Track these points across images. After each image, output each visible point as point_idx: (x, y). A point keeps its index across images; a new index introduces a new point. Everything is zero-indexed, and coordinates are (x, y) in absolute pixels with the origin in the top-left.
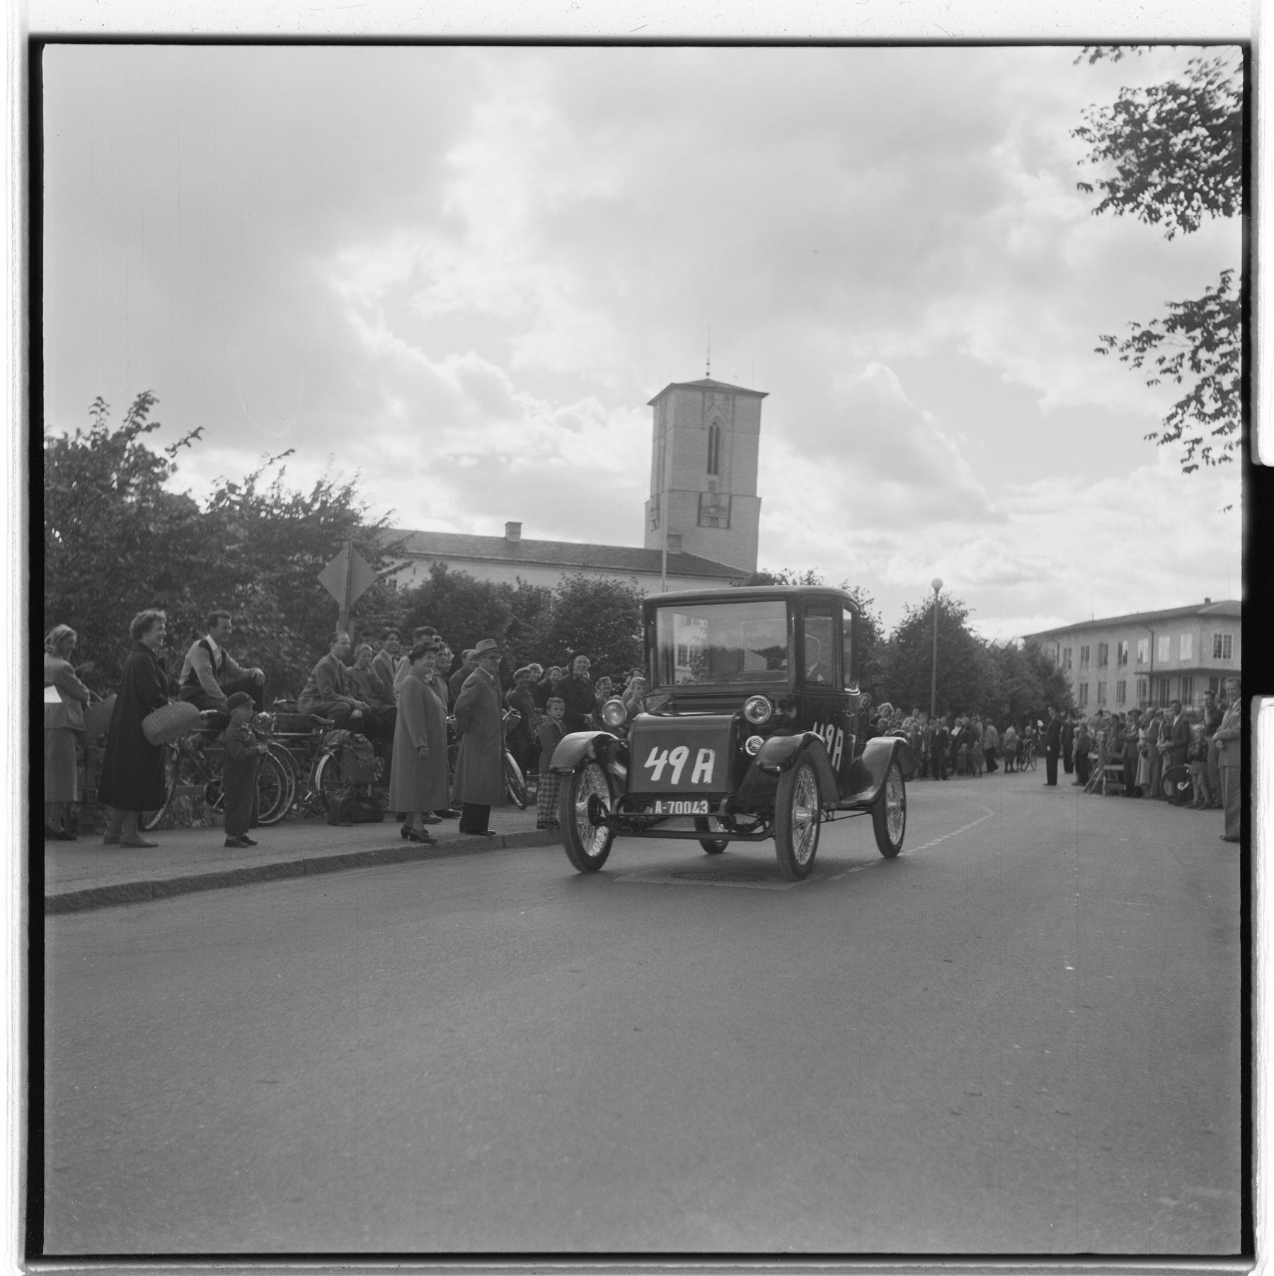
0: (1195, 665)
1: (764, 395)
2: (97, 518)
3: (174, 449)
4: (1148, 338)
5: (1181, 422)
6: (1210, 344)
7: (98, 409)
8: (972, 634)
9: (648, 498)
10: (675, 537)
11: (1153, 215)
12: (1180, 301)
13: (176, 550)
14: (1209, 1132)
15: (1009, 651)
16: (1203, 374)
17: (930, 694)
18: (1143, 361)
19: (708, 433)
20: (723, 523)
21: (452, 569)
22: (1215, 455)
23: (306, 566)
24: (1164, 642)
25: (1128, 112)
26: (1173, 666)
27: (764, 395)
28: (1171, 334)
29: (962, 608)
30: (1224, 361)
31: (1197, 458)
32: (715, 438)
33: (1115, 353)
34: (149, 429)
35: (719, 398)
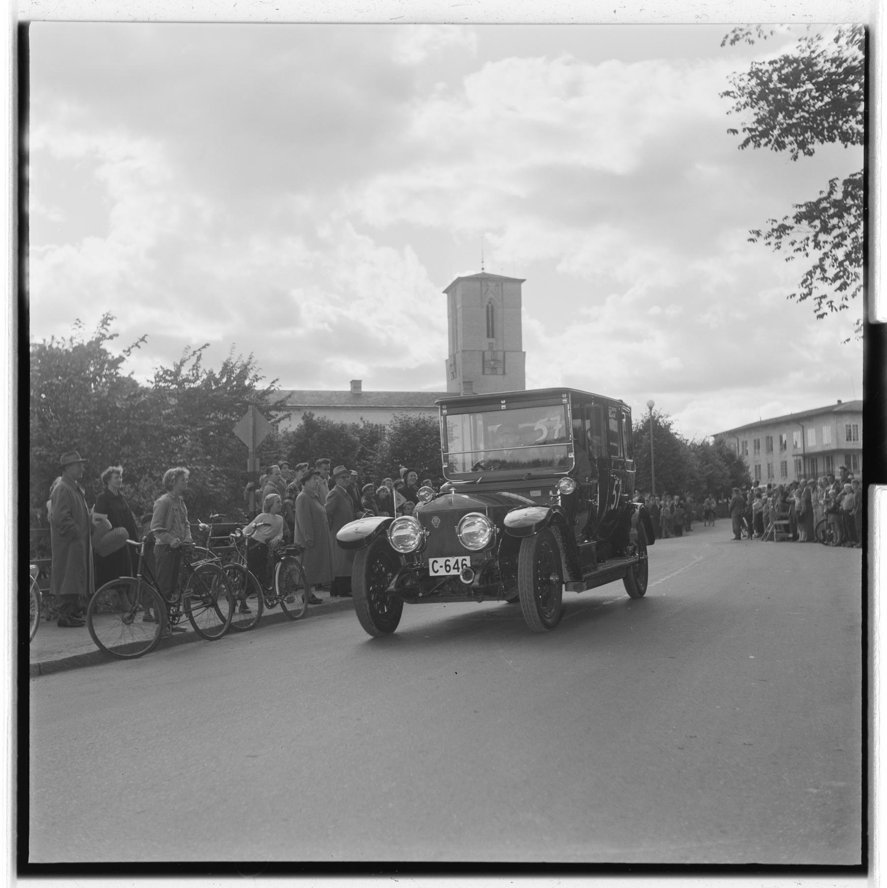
0: (834, 447)
1: (523, 281)
2: (79, 400)
3: (129, 350)
4: (783, 229)
5: (811, 284)
6: (826, 229)
7: (77, 327)
8: (677, 437)
9: (447, 358)
10: (468, 383)
11: (781, 146)
12: (802, 203)
13: (134, 418)
14: (840, 750)
15: (704, 446)
16: (823, 251)
17: (651, 479)
18: (782, 245)
19: (486, 310)
20: (500, 371)
21: (318, 416)
22: (836, 305)
23: (219, 421)
24: (811, 433)
25: (758, 77)
26: (819, 449)
27: (523, 281)
28: (799, 225)
29: (669, 420)
30: (837, 240)
31: (825, 308)
32: (490, 313)
33: (761, 241)
34: (111, 338)
35: (492, 285)
